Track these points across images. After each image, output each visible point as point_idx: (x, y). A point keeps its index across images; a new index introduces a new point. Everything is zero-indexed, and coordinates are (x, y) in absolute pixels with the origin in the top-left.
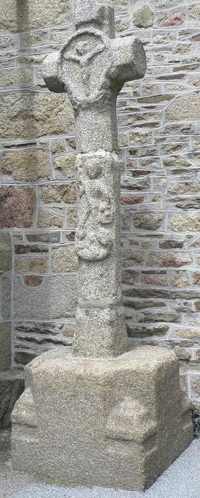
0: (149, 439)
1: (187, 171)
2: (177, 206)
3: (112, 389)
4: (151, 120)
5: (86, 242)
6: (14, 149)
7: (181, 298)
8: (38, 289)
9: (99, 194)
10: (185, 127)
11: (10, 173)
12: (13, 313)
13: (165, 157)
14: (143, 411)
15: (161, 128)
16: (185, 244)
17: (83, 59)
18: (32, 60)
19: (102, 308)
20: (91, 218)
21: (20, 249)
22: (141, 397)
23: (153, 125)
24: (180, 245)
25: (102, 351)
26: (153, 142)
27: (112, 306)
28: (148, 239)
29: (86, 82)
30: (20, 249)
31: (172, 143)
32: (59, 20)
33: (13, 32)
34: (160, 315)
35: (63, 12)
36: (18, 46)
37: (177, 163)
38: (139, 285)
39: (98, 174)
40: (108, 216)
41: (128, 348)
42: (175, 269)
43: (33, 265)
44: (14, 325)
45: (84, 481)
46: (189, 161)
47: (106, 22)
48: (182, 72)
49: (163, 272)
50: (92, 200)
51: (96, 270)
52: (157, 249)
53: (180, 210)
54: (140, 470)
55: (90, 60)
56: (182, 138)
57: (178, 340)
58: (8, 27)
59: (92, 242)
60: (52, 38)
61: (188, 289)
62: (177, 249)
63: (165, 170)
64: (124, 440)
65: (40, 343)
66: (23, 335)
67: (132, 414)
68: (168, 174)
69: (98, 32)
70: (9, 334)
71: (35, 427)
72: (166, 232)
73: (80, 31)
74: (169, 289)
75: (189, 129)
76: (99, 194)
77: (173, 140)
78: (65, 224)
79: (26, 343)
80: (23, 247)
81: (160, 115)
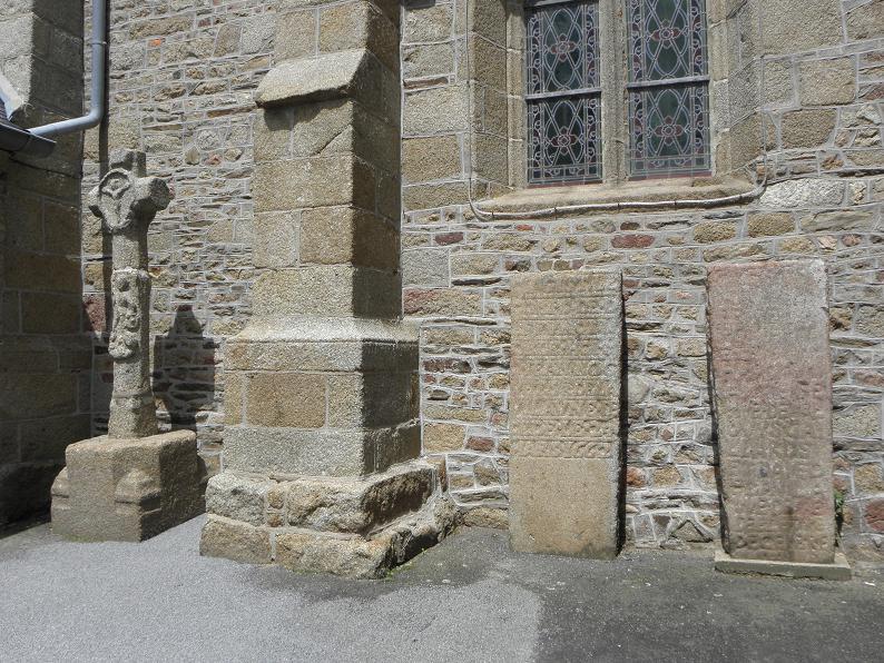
0: (146, 503)
1: (222, 284)
4: (197, 241)
11: (92, 283)
12: (92, 407)
17: (115, 193)
22: (147, 469)
23: (198, 245)
27: (136, 397)
28: (195, 341)
33: (96, 162)
38: (188, 380)
39: (125, 287)
44: (93, 417)
45: (100, 538)
48: (218, 203)
49: (205, 369)
52: (201, 349)
53: (217, 317)
54: (138, 526)
55: (120, 195)
57: (214, 425)
58: (92, 158)
63: (207, 283)
69: (126, 172)
71: (67, 497)
72: (206, 335)
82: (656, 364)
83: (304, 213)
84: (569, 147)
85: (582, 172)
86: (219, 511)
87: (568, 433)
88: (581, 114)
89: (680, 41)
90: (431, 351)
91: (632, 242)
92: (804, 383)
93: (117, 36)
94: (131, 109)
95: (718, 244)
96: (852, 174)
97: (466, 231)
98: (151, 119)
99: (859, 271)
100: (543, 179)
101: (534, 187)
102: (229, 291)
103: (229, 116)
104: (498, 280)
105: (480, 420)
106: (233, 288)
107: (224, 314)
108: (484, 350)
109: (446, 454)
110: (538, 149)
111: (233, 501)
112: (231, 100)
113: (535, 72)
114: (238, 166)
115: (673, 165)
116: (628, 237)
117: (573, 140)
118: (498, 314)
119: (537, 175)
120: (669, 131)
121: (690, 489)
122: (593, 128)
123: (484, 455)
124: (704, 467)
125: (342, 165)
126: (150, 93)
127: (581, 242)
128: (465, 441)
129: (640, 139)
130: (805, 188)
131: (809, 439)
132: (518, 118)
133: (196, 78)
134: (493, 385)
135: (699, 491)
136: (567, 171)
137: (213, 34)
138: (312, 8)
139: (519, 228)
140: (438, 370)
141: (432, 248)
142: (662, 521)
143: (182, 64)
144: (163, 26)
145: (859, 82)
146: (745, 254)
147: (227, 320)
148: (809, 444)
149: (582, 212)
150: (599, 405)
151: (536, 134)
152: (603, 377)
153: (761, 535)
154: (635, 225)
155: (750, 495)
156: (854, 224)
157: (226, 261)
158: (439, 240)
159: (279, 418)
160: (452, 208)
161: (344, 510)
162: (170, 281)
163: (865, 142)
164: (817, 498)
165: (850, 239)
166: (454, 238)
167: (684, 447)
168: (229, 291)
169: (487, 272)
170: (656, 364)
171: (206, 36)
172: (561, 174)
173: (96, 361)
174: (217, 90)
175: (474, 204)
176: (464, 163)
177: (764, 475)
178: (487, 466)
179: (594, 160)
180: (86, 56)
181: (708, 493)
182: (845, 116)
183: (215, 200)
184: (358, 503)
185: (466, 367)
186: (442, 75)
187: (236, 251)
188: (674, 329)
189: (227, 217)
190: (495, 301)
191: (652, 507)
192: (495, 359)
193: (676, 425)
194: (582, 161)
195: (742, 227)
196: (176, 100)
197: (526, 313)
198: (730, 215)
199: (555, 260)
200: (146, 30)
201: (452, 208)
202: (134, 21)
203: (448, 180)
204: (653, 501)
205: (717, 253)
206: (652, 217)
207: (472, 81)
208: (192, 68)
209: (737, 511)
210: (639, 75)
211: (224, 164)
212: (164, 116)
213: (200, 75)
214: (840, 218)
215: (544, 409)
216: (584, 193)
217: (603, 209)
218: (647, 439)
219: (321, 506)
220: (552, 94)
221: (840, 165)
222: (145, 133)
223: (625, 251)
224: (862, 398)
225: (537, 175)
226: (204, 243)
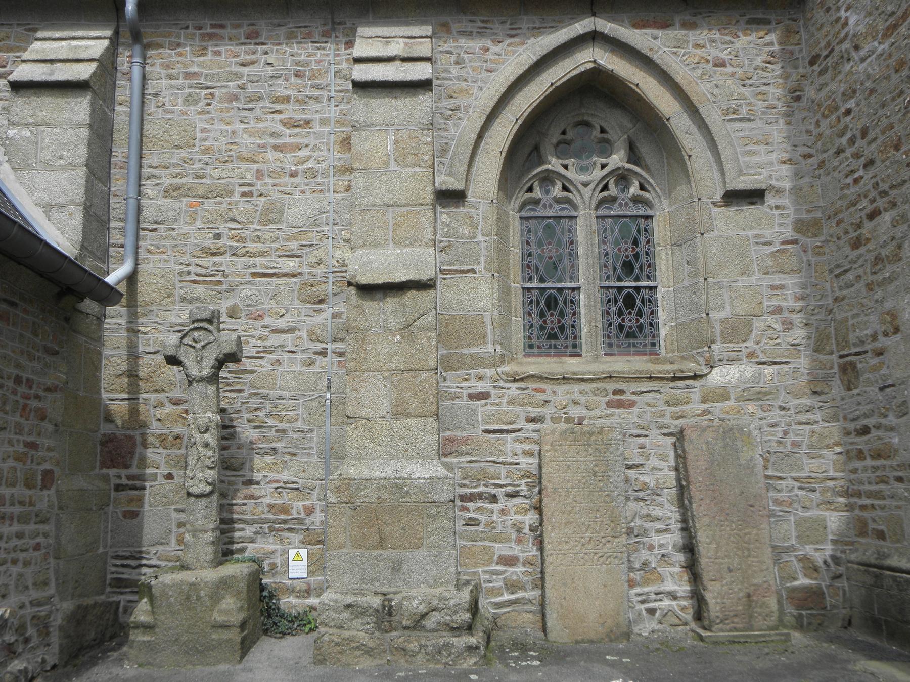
0: (243, 626)
3: (224, 584)
4: (238, 388)
5: (195, 482)
6: (118, 402)
7: (258, 523)
8: (135, 521)
9: (207, 445)
13: (248, 416)
14: (239, 605)
15: (246, 394)
18: (139, 331)
19: (206, 532)
20: (199, 463)
21: (118, 488)
24: (258, 483)
25: (205, 565)
26: (239, 404)
28: (233, 479)
29: (199, 362)
30: (118, 488)
32: (164, 302)
34: (240, 538)
35: (168, 297)
36: (125, 317)
41: (221, 563)
43: (131, 500)
46: (266, 420)
47: (216, 321)
48: (262, 354)
49: (245, 504)
50: (201, 449)
51: (203, 502)
55: (203, 347)
59: (200, 481)
60: (157, 316)
61: (263, 516)
62: (256, 486)
63: (247, 425)
64: (225, 627)
65: (134, 568)
66: (119, 562)
67: (231, 608)
69: (210, 327)
70: (105, 563)
73: (196, 325)
74: (248, 517)
76: (207, 445)
77: (254, 403)
78: (162, 466)
79: (121, 570)
80: (122, 485)
81: (245, 384)
82: (641, 494)
83: (395, 376)
84: (556, 326)
85: (566, 347)
86: (332, 624)
87: (589, 547)
88: (565, 302)
89: (636, 256)
90: (465, 486)
91: (620, 404)
92: (751, 506)
93: (149, 192)
94: (165, 261)
95: (680, 408)
96: (764, 363)
97: (493, 391)
98: (189, 273)
99: (772, 429)
100: (536, 350)
101: (529, 356)
102: (272, 434)
103: (274, 279)
104: (520, 430)
105: (508, 540)
106: (277, 431)
107: (266, 453)
108: (510, 485)
109: (480, 570)
110: (532, 326)
111: (346, 615)
112: (275, 265)
113: (528, 267)
114: (282, 323)
115: (634, 346)
116: (618, 400)
117: (559, 322)
118: (521, 456)
119: (531, 346)
120: (630, 321)
121: (669, 586)
122: (574, 314)
123: (511, 569)
124: (677, 569)
125: (428, 341)
126: (188, 249)
127: (583, 402)
128: (495, 558)
129: (610, 325)
130: (736, 371)
131: (757, 544)
132: (517, 301)
133: (238, 241)
134: (516, 513)
135: (676, 588)
136: (555, 345)
137: (257, 205)
138: (385, 208)
139: (536, 390)
140: (472, 501)
141: (465, 402)
142: (652, 612)
143: (224, 227)
144: (201, 191)
145: (766, 303)
146: (699, 415)
147: (268, 459)
148: (758, 548)
149: (583, 380)
150: (612, 524)
151: (530, 314)
152: (614, 504)
153: (731, 614)
154: (622, 392)
155: (722, 586)
156: (768, 397)
157: (268, 406)
158: (471, 396)
159: (382, 542)
160: (481, 371)
161: (456, 612)
163: (771, 342)
164: (765, 585)
165: (766, 407)
166: (484, 396)
167: (663, 556)
168: (272, 434)
169: (511, 423)
170: (641, 494)
171: (248, 206)
172: (550, 347)
173: (115, 500)
174: (261, 254)
175: (499, 370)
176: (490, 337)
177: (730, 571)
178: (515, 578)
179: (575, 338)
180: (112, 205)
181: (683, 588)
182: (758, 324)
183: (261, 358)
184: (467, 606)
185: (494, 498)
186: (471, 267)
187: (280, 398)
188: (653, 468)
189: (272, 367)
190: (518, 447)
191: (643, 602)
192: (518, 492)
193: (656, 539)
194: (566, 338)
195: (696, 396)
196: (216, 259)
197: (554, 456)
198: (687, 387)
199: (564, 416)
200: (182, 191)
201: (481, 371)
202: (168, 181)
203: (477, 350)
204: (644, 597)
205: (680, 414)
206: (634, 387)
207: (496, 275)
208: (235, 232)
209: (714, 598)
210: (608, 278)
211: (267, 321)
212: (203, 272)
213: (242, 240)
214: (759, 393)
215: (570, 530)
216: (572, 365)
217: (599, 379)
218: (636, 550)
219: (434, 610)
220: (543, 285)
221: (757, 356)
222: (181, 284)
223: (617, 411)
224: (779, 516)
225: (531, 346)
226: (246, 389)
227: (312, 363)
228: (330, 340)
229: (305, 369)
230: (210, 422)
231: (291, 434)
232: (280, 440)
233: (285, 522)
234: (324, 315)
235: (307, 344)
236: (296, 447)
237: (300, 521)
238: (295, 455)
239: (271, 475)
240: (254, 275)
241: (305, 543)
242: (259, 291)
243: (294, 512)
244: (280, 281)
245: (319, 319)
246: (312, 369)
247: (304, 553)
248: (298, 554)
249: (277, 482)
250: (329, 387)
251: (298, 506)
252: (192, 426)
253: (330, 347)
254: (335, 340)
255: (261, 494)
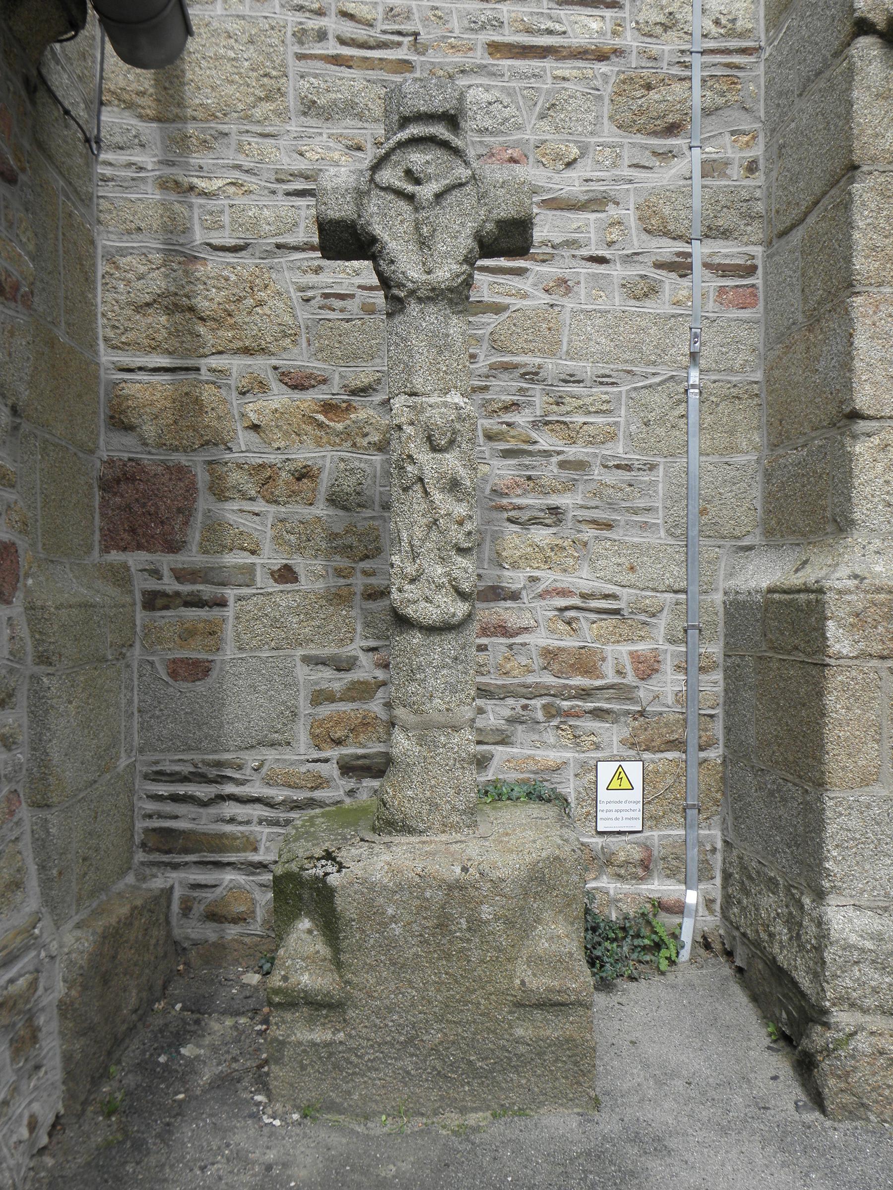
1: (530, 453)
2: (509, 520)
10: (529, 369)
16: (524, 593)
20: (434, 535)
24: (514, 596)
31: (503, 398)
37: (513, 437)
40: (470, 533)
42: (503, 640)
46: (534, 435)
56: (521, 389)
59: (439, 587)
62: (509, 604)
68: (492, 456)
75: (537, 374)
77: (504, 390)
98: (322, 35)
102: (549, 471)
103: (548, 64)
106: (562, 465)
107: (534, 521)
112: (550, 25)
114: (571, 184)
147: (541, 535)
162: (375, 437)
168: (549, 471)
187: (571, 379)
227: (652, 291)
228: (697, 230)
229: (632, 306)
230: (460, 419)
231: (597, 472)
232: (569, 487)
233: (585, 694)
234: (678, 167)
235: (637, 241)
236: (612, 506)
237: (623, 692)
238: (609, 526)
239: (549, 578)
240: (495, 48)
241: (636, 746)
242: (510, 92)
243: (608, 669)
244: (566, 69)
245: (666, 176)
246: (651, 307)
247: (634, 770)
248: (620, 774)
249: (564, 593)
250: (694, 356)
251: (617, 655)
252: (409, 430)
253: (699, 251)
254: (711, 233)
255: (524, 623)
